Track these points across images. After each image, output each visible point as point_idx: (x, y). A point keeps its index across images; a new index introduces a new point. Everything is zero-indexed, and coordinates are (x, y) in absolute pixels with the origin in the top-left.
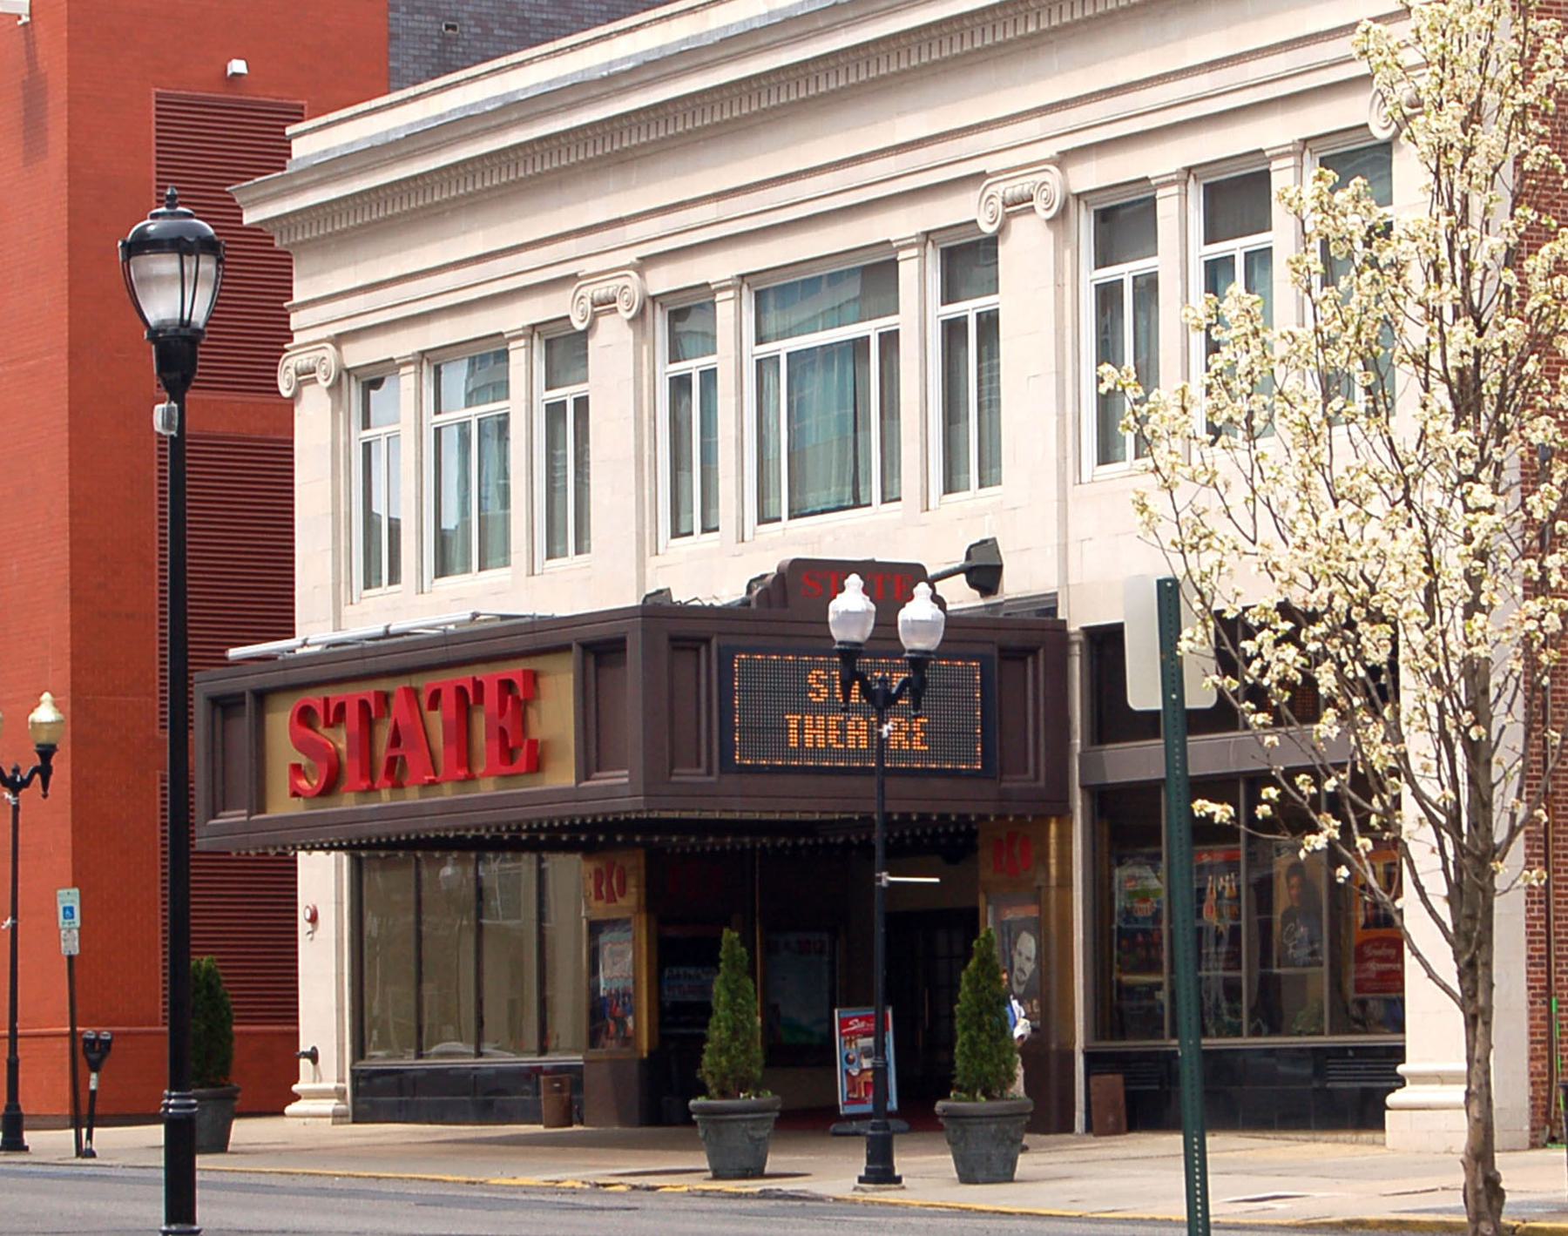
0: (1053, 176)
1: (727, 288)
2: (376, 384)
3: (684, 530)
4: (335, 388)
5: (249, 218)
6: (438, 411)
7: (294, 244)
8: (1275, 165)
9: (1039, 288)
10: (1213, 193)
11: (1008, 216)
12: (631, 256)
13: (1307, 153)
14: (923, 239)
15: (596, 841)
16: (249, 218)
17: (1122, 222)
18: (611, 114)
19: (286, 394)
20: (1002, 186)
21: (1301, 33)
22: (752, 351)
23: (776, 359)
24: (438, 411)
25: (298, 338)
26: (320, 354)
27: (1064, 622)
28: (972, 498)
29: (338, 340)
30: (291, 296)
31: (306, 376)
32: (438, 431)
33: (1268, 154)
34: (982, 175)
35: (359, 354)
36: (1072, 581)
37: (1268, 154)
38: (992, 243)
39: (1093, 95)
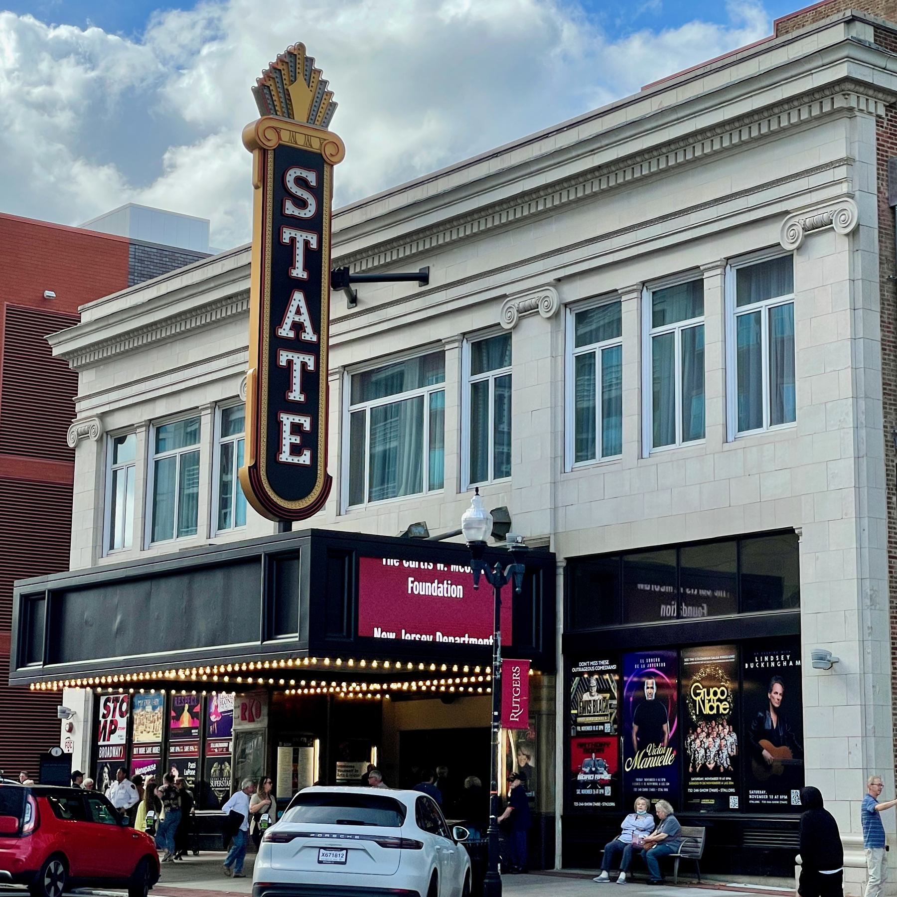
0: (552, 294)
1: (206, 409)
2: (121, 440)
3: (692, 432)
4: (100, 440)
5: (56, 352)
6: (157, 452)
7: (80, 367)
8: (706, 275)
9: (540, 364)
10: (477, 347)
11: (520, 318)
12: (551, 277)
13: (728, 266)
14: (342, 370)
15: (237, 677)
16: (56, 352)
17: (596, 318)
18: (699, 127)
19: (71, 445)
20: (518, 301)
21: (729, 192)
22: (649, 331)
23: (592, 355)
24: (157, 452)
25: (79, 417)
26: (92, 423)
27: (554, 554)
28: (491, 484)
29: (102, 416)
30: (77, 394)
31: (83, 436)
32: (157, 462)
33: (620, 292)
34: (505, 296)
35: (118, 421)
36: (560, 530)
37: (702, 268)
38: (506, 339)
39: (827, 165)
